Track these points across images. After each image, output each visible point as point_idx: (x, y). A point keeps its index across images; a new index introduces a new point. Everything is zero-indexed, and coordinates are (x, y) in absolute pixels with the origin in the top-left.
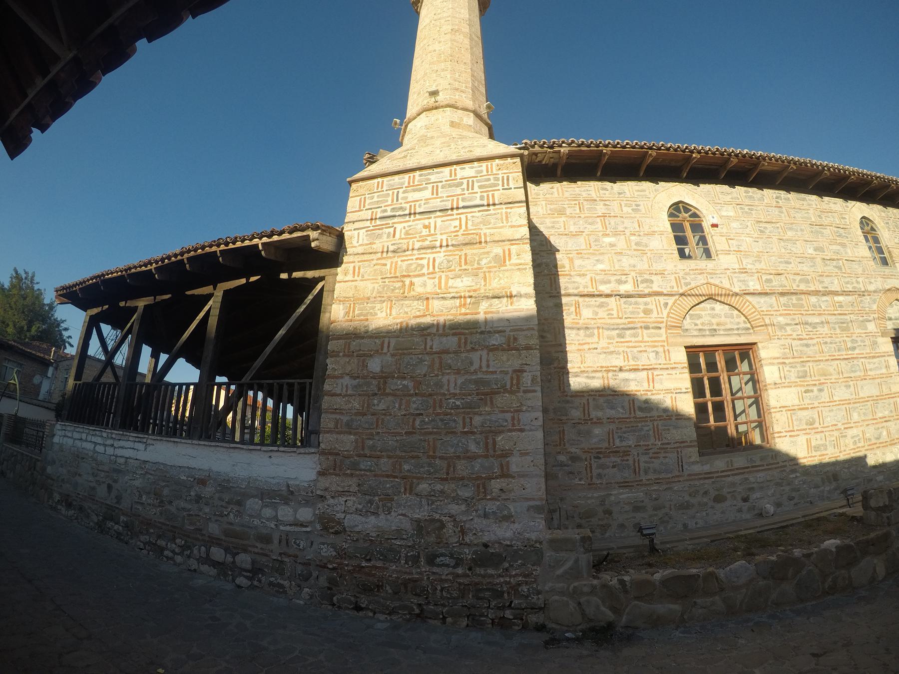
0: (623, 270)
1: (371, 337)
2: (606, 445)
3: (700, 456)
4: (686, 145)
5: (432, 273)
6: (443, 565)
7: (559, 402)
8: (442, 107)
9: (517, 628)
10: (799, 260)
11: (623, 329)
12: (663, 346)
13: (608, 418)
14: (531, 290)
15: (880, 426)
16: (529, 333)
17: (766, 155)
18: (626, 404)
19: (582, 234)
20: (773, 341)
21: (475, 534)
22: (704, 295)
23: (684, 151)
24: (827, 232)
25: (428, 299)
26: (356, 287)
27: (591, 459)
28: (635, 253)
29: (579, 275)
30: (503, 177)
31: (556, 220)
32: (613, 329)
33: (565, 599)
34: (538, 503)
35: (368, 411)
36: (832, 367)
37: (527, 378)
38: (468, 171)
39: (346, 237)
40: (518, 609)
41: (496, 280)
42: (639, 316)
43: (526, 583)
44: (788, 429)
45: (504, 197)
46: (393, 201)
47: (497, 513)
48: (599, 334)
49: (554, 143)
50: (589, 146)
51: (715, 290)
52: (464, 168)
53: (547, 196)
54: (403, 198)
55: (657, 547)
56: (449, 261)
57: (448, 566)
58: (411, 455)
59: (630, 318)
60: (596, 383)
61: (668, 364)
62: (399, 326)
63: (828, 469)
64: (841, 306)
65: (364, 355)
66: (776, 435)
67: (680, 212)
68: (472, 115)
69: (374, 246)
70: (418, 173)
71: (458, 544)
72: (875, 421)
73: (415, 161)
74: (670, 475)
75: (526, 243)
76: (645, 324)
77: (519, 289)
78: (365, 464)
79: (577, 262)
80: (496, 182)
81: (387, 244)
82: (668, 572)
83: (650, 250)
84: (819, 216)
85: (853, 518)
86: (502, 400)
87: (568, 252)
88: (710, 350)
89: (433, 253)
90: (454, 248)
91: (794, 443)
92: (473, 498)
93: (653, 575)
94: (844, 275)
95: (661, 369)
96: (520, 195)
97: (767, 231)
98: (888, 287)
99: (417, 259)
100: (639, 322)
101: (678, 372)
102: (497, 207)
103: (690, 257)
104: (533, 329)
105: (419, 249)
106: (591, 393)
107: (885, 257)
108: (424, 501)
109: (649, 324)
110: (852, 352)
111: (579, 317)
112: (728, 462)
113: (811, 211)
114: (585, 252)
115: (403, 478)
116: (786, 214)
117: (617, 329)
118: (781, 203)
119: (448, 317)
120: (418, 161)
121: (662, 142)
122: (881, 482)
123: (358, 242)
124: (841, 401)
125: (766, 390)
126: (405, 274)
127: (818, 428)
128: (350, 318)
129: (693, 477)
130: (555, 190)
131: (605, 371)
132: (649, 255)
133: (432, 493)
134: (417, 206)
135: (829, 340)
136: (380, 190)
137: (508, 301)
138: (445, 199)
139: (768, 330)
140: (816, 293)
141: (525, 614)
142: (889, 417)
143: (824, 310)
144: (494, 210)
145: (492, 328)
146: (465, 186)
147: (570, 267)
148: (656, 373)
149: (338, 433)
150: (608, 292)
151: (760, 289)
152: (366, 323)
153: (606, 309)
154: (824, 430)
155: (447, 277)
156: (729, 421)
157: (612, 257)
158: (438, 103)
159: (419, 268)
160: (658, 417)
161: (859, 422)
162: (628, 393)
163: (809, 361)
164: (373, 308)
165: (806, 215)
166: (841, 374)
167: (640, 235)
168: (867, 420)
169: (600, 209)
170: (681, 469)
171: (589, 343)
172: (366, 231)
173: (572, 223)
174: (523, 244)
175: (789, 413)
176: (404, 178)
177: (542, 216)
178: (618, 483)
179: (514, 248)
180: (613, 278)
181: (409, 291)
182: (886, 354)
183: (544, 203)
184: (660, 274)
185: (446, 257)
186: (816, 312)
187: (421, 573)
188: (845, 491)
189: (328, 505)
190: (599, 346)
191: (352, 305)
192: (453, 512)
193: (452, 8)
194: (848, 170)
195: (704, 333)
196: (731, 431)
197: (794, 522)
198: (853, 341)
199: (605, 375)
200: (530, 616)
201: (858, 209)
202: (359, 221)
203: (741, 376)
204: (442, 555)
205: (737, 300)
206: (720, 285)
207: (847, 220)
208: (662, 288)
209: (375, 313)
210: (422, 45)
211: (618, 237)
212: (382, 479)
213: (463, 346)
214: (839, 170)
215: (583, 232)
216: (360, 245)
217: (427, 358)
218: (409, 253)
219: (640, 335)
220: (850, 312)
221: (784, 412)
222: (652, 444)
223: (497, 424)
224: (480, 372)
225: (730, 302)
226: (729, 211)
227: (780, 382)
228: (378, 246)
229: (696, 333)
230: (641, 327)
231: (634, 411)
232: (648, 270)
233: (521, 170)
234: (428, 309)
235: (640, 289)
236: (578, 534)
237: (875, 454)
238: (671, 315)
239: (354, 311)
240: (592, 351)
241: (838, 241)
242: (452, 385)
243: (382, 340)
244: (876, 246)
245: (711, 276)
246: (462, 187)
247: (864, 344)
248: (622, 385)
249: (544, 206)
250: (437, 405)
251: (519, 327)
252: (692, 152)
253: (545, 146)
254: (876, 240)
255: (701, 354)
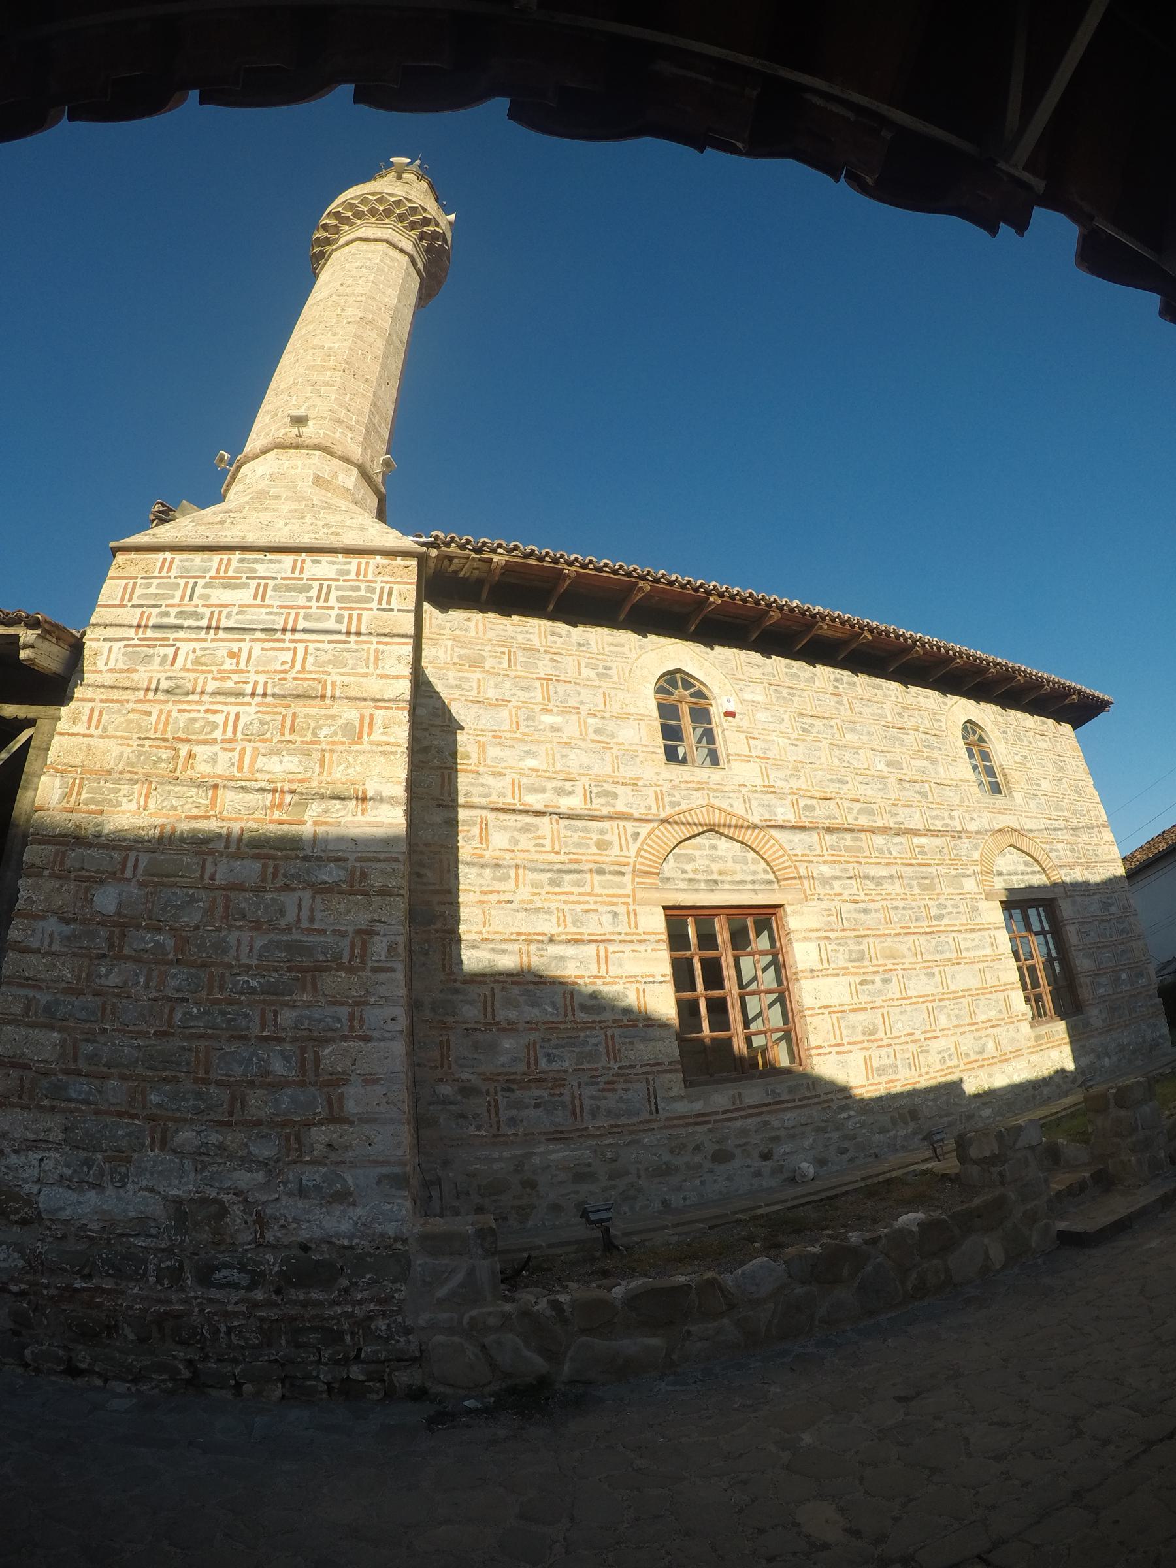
0: (569, 773)
1: (104, 846)
2: (522, 1067)
3: (685, 1087)
4: (701, 581)
5: (231, 741)
6: (229, 1285)
7: (441, 991)
8: (307, 446)
9: (374, 1397)
10: (861, 779)
11: (560, 871)
12: (627, 904)
13: (527, 1023)
14: (400, 792)
15: (984, 1033)
16: (388, 867)
17: (826, 613)
18: (559, 1000)
19: (506, 705)
20: (811, 903)
21: (283, 1226)
22: (701, 825)
23: (696, 590)
24: (910, 738)
25: (216, 787)
26: (89, 747)
27: (496, 1092)
28: (593, 745)
29: (493, 774)
30: (382, 588)
31: (466, 675)
32: (543, 870)
33: (456, 1339)
34: (396, 1170)
35: (87, 986)
36: (905, 945)
37: (379, 946)
38: (324, 567)
39: (86, 652)
40: (373, 1362)
41: (341, 768)
42: (589, 851)
43: (384, 1314)
44: (833, 1042)
45: (378, 623)
46: (182, 599)
47: (322, 1187)
48: (517, 876)
49: (484, 544)
50: (541, 559)
51: (720, 817)
52: (319, 562)
53: (458, 632)
54: (201, 597)
55: (617, 1242)
56: (262, 723)
57: (236, 1286)
58: (164, 1074)
59: (574, 854)
60: (508, 962)
61: (634, 934)
62: (157, 832)
63: (901, 1102)
64: (923, 853)
65: (89, 879)
66: (814, 1052)
67: (676, 688)
68: (355, 471)
69: (135, 676)
70: (238, 555)
71: (253, 1246)
72: (975, 1027)
73: (238, 533)
74: (635, 1120)
75: (403, 709)
76: (598, 865)
77: (379, 787)
78: (79, 1088)
79: (493, 752)
80: (369, 595)
81: (159, 675)
82: (636, 1283)
83: (617, 744)
84: (900, 714)
85: (944, 1177)
86: (331, 982)
87: (479, 733)
88: (705, 915)
89: (237, 704)
90: (276, 701)
91: (844, 1064)
92: (277, 1161)
93: (610, 1290)
94: (930, 805)
95: (620, 942)
96: (407, 623)
97: (814, 731)
98: (998, 827)
99: (207, 711)
100: (587, 861)
101: (649, 948)
102: (362, 638)
103: (684, 761)
104: (396, 860)
105: (213, 694)
106: (498, 978)
107: (997, 783)
108: (188, 1165)
109: (604, 866)
110: (938, 923)
111: (485, 846)
112: (733, 1096)
113: (888, 706)
114: (508, 735)
115: (150, 1118)
116: (848, 707)
117: (548, 871)
118: (841, 689)
119: (248, 825)
120: (242, 534)
121: (663, 571)
122: (988, 1117)
123: (106, 664)
124: (920, 996)
125: (797, 980)
126: (181, 735)
127: (882, 1040)
128: (71, 805)
129: (675, 1122)
130: (472, 624)
131: (525, 940)
132: (615, 751)
133: (203, 1149)
134: (224, 615)
135: (901, 904)
136: (164, 574)
137: (357, 806)
138: (275, 610)
139: (803, 885)
140: (885, 831)
141: (388, 1370)
142: (997, 1019)
143: (896, 858)
144: (356, 642)
145: (324, 851)
146: (313, 593)
147: (479, 758)
148: (611, 948)
149: (32, 1026)
150: (539, 807)
151: (794, 820)
152: (99, 819)
153: (534, 835)
154: (892, 1042)
155: (256, 753)
156: (736, 1029)
157: (552, 749)
158: (302, 439)
159: (208, 729)
160: (614, 1021)
161: (949, 1029)
162: (562, 980)
163: (868, 936)
164: (115, 792)
165: (879, 711)
166: (919, 957)
167: (603, 718)
168: (962, 1026)
169: (544, 666)
170: (654, 1109)
171: (499, 892)
172: (126, 646)
173: (492, 683)
174: (397, 709)
175: (835, 1016)
176: (211, 560)
177: (442, 665)
178: (544, 1133)
179: (380, 715)
180: (550, 785)
181: (185, 768)
182: (991, 926)
183: (449, 643)
184: (630, 784)
185: (260, 715)
186: (882, 861)
187: (186, 1301)
188: (928, 1137)
189: (7, 1167)
190: (517, 898)
191: (77, 782)
192: (242, 1185)
193: (373, 282)
194: (953, 649)
195: (696, 886)
196: (739, 1045)
197: (847, 1188)
198: (940, 906)
199: (524, 948)
200: (397, 1373)
201: (961, 708)
202: (116, 625)
203: (756, 957)
204: (226, 1266)
205: (754, 835)
206: (729, 809)
207: (943, 724)
208: (631, 808)
209: (117, 801)
210: (303, 332)
211: (567, 716)
212: (109, 1120)
213: (269, 878)
214: (939, 648)
215: (509, 701)
216: (110, 671)
217: (203, 895)
218: (196, 698)
219: (588, 883)
220: (937, 862)
221: (827, 1016)
222: (603, 1068)
223: (322, 1025)
224: (297, 929)
225: (744, 837)
226: (757, 694)
227: (820, 967)
228: (141, 677)
229: (683, 885)
230: (591, 870)
231: (573, 1010)
232: (611, 777)
233: (415, 581)
234: (213, 805)
235: (594, 806)
236: (472, 1225)
237: (977, 1077)
238: (643, 853)
239: (79, 793)
240: (503, 905)
241: (926, 754)
242: (245, 949)
243: (124, 853)
244: (984, 766)
245: (716, 794)
246: (309, 594)
247: (958, 910)
248: (553, 965)
249: (449, 648)
250: (216, 984)
251: (372, 855)
252: (709, 593)
253: (469, 547)
254: (986, 756)
255: (690, 919)
